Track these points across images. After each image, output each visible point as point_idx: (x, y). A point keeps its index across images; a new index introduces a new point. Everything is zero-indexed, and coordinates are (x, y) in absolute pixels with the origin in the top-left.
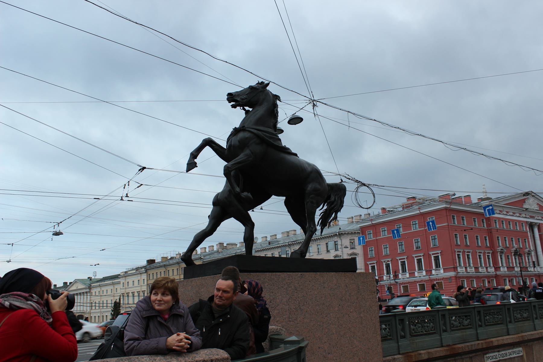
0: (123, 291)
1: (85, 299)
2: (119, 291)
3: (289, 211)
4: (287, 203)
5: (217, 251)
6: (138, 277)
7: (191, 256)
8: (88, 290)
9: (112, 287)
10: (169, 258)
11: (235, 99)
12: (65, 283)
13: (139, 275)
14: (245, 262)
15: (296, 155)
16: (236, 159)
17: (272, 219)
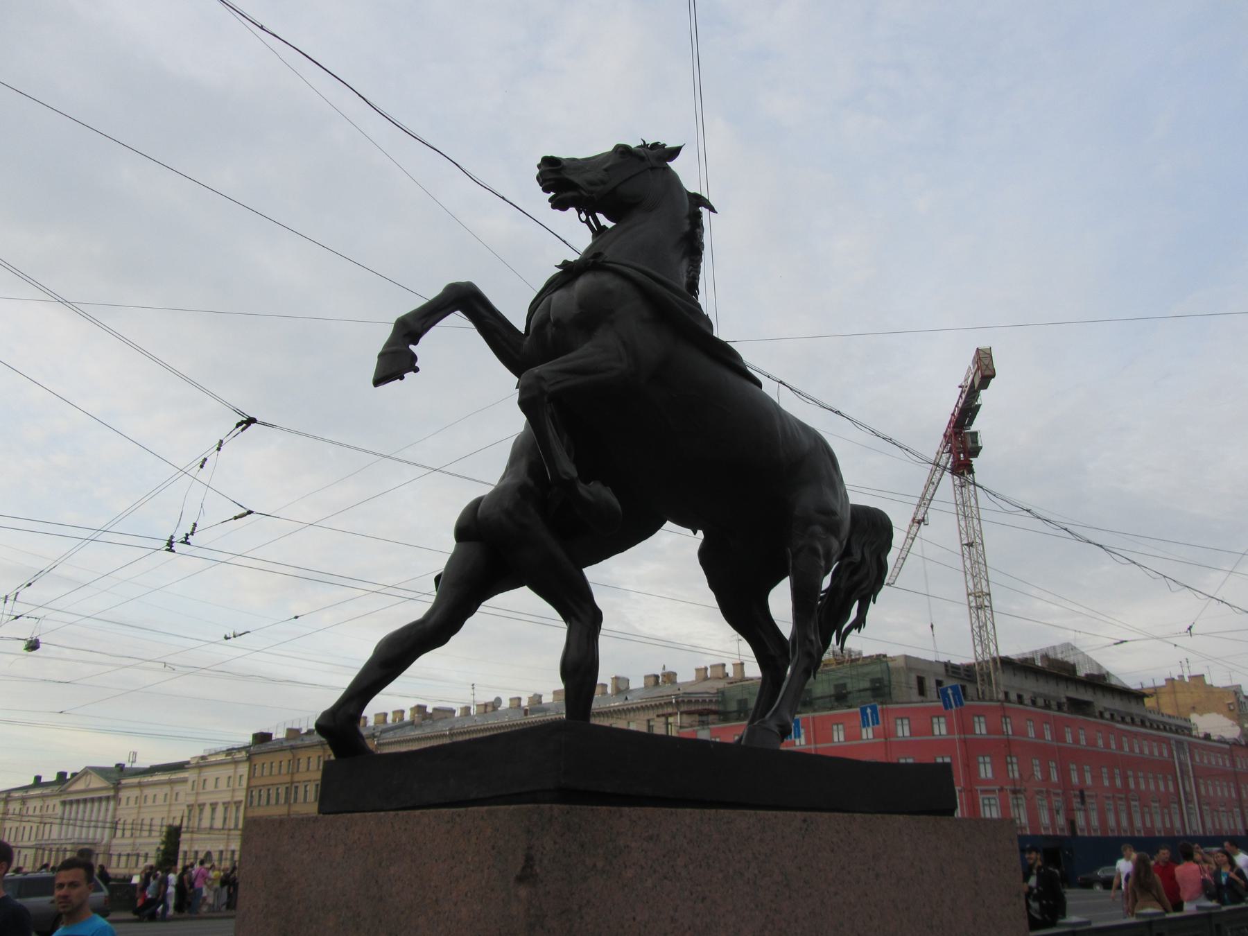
0: (191, 800)
1: (102, 814)
2: (182, 798)
3: (713, 585)
4: (707, 557)
5: (412, 723)
6: (230, 770)
7: (356, 716)
8: (112, 793)
9: (167, 789)
10: (304, 731)
11: (562, 181)
12: (62, 775)
13: (232, 766)
14: (576, 759)
15: (759, 384)
16: (570, 355)
17: (662, 610)
